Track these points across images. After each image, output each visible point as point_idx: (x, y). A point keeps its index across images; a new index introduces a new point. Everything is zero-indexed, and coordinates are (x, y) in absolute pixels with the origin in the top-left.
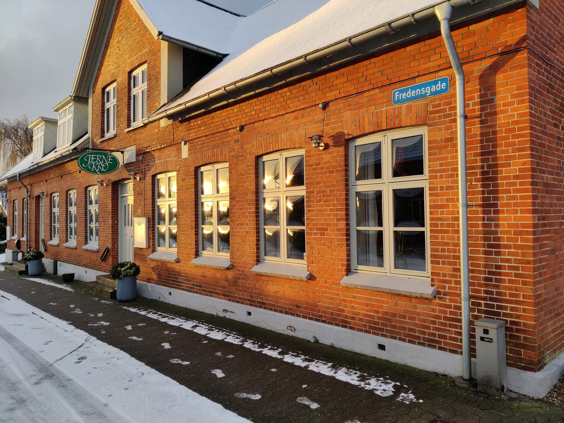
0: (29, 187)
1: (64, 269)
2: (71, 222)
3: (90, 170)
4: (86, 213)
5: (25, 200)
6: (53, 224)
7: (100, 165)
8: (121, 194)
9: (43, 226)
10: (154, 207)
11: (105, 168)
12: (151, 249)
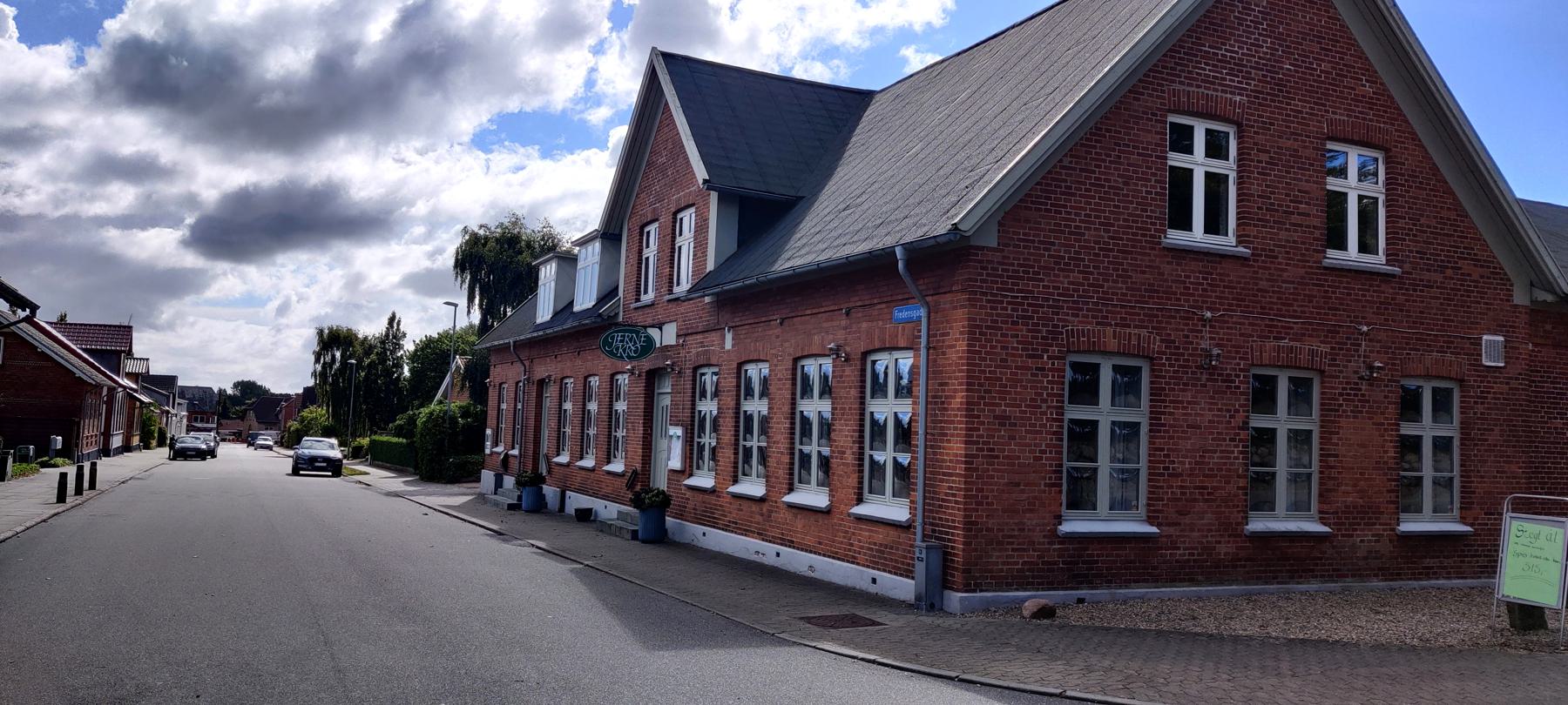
1: (576, 501)
4: (610, 415)
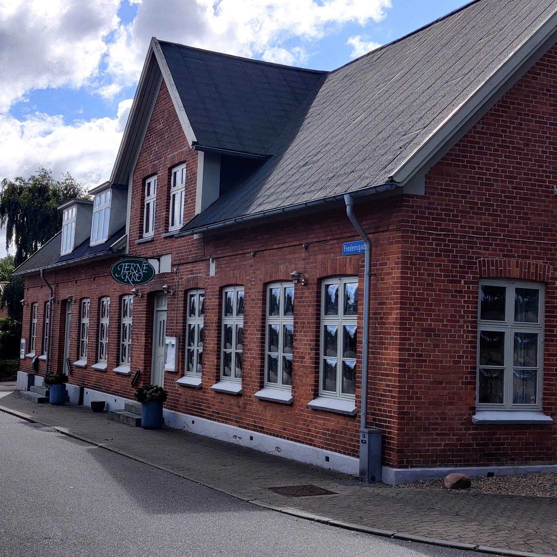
0: (53, 287)
1: (93, 396)
2: (102, 336)
3: (123, 281)
4: (119, 327)
5: (49, 303)
6: (81, 339)
7: (134, 274)
8: (157, 307)
9: (69, 341)
10: (185, 326)
11: (139, 278)
12: (180, 373)
